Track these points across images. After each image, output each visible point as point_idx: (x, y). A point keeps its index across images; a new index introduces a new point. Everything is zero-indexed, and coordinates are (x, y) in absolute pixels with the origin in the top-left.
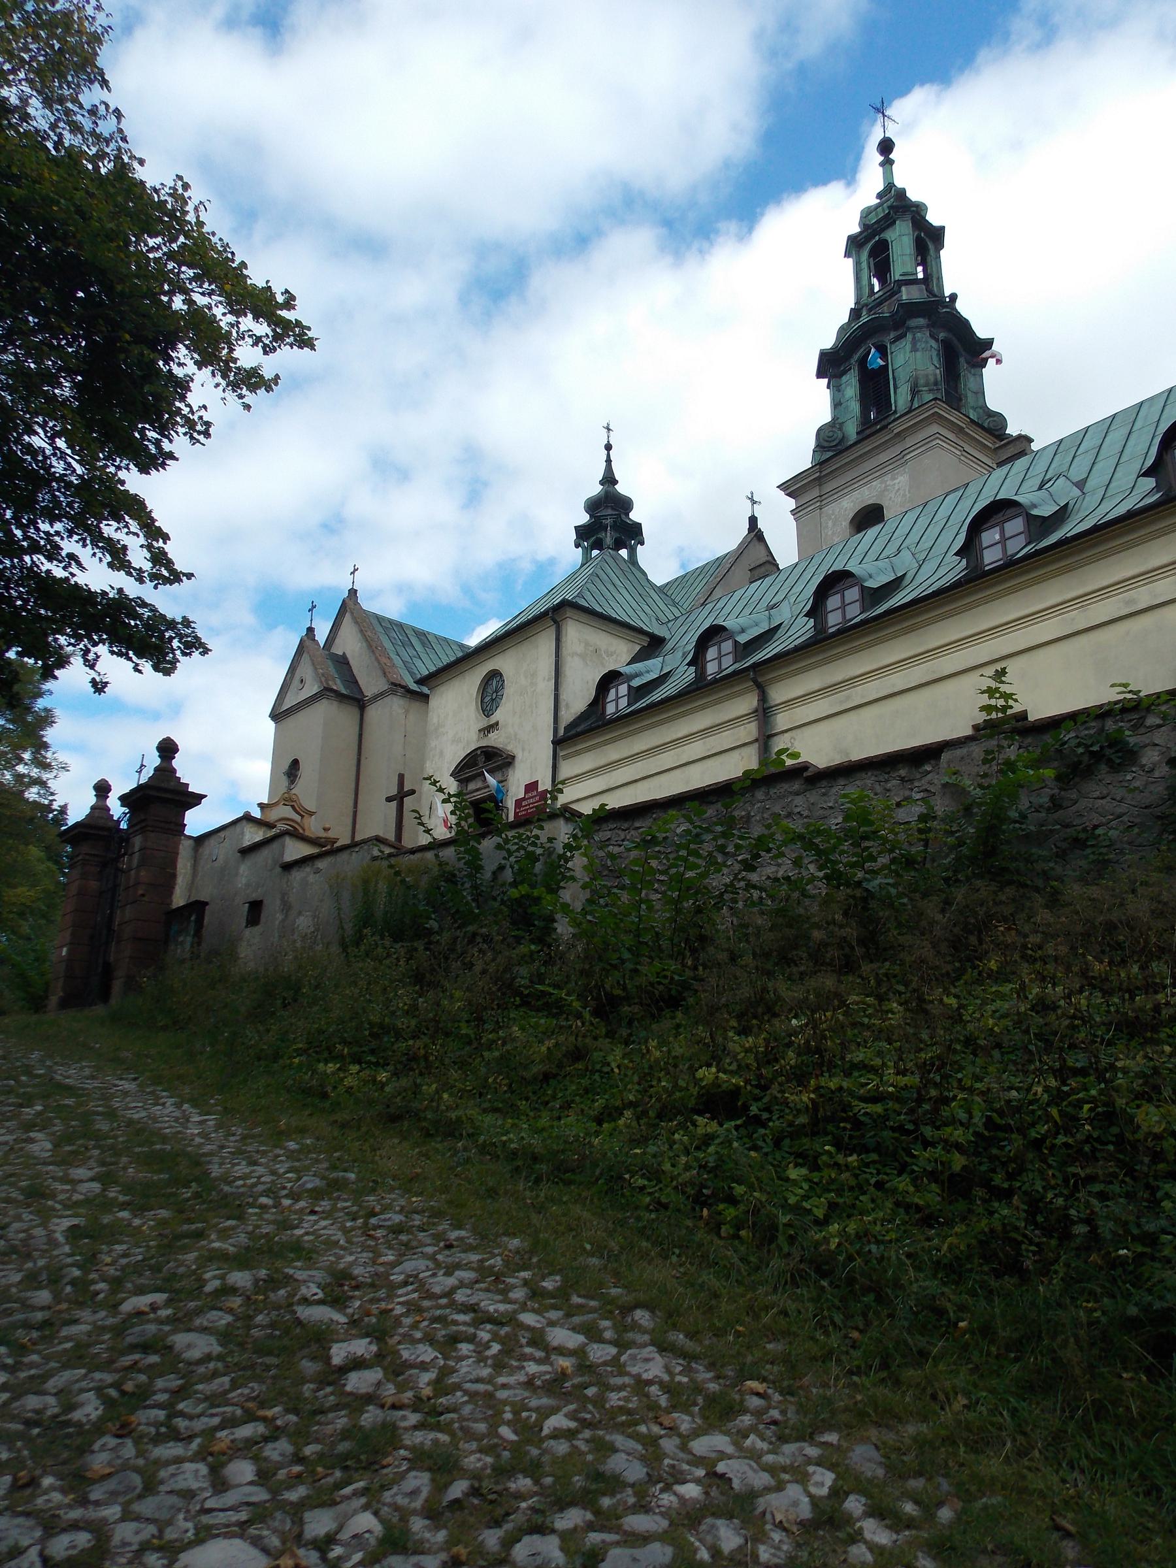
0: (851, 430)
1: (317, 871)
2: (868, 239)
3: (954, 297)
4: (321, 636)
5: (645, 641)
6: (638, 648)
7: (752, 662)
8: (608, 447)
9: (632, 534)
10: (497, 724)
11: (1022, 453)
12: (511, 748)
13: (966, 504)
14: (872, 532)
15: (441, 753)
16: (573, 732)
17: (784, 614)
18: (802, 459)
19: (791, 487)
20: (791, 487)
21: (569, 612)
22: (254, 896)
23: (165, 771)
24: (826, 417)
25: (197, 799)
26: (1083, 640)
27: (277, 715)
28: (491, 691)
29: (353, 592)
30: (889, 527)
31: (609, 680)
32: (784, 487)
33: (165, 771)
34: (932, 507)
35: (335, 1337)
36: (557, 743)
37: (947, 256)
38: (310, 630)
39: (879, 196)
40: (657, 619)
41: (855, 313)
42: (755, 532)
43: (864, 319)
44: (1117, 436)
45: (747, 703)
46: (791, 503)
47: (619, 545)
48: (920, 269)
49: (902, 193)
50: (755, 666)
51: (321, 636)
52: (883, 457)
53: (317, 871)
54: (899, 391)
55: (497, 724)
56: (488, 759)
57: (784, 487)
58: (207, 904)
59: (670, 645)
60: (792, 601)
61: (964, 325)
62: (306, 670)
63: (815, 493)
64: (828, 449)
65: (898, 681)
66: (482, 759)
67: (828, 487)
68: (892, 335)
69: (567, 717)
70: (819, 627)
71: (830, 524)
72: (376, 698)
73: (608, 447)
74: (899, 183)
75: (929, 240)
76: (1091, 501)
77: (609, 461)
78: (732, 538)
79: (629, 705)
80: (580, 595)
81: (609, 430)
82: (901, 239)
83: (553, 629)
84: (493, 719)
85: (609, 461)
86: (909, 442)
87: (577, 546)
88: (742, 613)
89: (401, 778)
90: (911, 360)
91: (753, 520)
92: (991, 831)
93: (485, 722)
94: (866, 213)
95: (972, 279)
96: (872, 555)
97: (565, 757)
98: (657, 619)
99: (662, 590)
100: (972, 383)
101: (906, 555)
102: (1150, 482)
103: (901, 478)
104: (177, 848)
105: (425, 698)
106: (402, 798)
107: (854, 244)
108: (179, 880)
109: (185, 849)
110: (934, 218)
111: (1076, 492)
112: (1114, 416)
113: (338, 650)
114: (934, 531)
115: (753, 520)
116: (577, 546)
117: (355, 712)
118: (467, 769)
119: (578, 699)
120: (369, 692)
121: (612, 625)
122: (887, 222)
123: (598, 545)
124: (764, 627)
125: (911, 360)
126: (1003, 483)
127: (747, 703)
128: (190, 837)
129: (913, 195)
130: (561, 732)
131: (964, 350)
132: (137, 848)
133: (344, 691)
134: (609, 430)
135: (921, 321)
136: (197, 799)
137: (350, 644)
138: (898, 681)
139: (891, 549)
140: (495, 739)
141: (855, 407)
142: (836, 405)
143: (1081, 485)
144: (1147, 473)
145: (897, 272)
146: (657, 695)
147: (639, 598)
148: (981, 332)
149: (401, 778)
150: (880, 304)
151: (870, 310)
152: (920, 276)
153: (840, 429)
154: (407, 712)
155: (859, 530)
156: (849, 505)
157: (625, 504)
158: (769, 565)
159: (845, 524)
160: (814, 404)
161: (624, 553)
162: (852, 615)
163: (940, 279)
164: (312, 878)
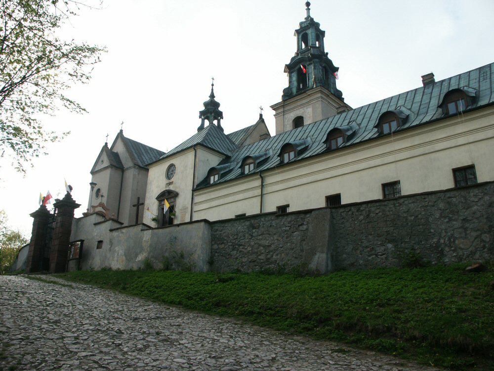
0: (294, 90)
1: (122, 233)
2: (302, 31)
3: (327, 54)
4: (109, 146)
5: (224, 157)
6: (222, 159)
7: (260, 169)
8: (213, 85)
9: (219, 115)
10: (173, 182)
11: (344, 111)
12: (177, 190)
13: (327, 125)
14: (299, 129)
15: (153, 191)
16: (199, 188)
17: (271, 153)
18: (279, 99)
19: (275, 107)
20: (275, 107)
21: (199, 147)
22: (100, 240)
23: (68, 196)
24: (287, 85)
25: (78, 206)
26: (357, 174)
27: (93, 172)
28: (170, 172)
29: (121, 131)
30: (305, 128)
31: (212, 171)
32: (272, 107)
33: (68, 196)
34: (318, 123)
35: (426, 88)
36: (194, 190)
37: (326, 40)
38: (106, 144)
39: (306, 18)
40: (228, 149)
41: (297, 54)
42: (262, 120)
43: (299, 57)
44: (370, 111)
45: (258, 183)
46: (274, 112)
47: (215, 118)
48: (317, 42)
49: (312, 19)
50: (261, 172)
51: (109, 146)
52: (304, 101)
53: (122, 233)
54: (310, 81)
55: (173, 182)
56: (168, 195)
57: (272, 107)
58: (84, 241)
59: (232, 159)
60: (273, 149)
61: (330, 62)
62: (105, 157)
63: (282, 110)
64: (287, 96)
65: (305, 180)
66: (167, 194)
67: (286, 109)
68: (308, 63)
69: (197, 182)
70: (282, 160)
71: (286, 121)
72: (127, 169)
73: (213, 85)
74: (312, 16)
75: (320, 35)
76: (362, 131)
77: (212, 90)
78: (254, 121)
79: (218, 180)
80: (203, 141)
81: (213, 79)
82: (311, 33)
83: (194, 151)
84: (171, 181)
85: (212, 90)
86: (312, 98)
87: (200, 118)
88: (256, 150)
89: (139, 198)
90: (312, 73)
91: (261, 115)
92: (210, 263)
93: (168, 181)
94: (301, 24)
95: (333, 49)
96: (298, 138)
97: (197, 195)
98: (228, 149)
99: (228, 136)
100: (332, 81)
101: (309, 139)
102: (376, 130)
103: (309, 109)
104: (72, 222)
105: (147, 170)
106: (139, 206)
107: (298, 32)
108: (72, 232)
109: (74, 222)
110: (322, 28)
111: (358, 127)
112: (370, 104)
113: (115, 150)
114: (318, 132)
115: (261, 115)
116: (200, 118)
117: (120, 172)
118: (161, 197)
119: (201, 177)
120: (126, 166)
121: (212, 151)
122: (307, 28)
123: (207, 118)
124: (227, 170)
125: (312, 73)
126: (340, 122)
127: (258, 183)
128: (75, 218)
129: (316, 20)
130: (195, 187)
131: (329, 70)
132: (59, 221)
133: (117, 166)
134: (213, 79)
135: (317, 60)
136: (78, 206)
137: (120, 149)
138: (305, 180)
139: (305, 136)
140: (171, 188)
141: (295, 84)
142: (290, 82)
143: (359, 125)
144: (375, 127)
145: (310, 43)
146: (228, 178)
147: (222, 141)
148: (336, 64)
149: (139, 198)
150: (304, 52)
151: (301, 54)
152: (317, 45)
153: (291, 90)
154: (138, 174)
155: (296, 128)
156: (292, 115)
157: (217, 105)
158: (267, 135)
159: (291, 121)
160: (283, 81)
161: (215, 122)
162: (293, 154)
163: (323, 47)
164: (120, 235)
